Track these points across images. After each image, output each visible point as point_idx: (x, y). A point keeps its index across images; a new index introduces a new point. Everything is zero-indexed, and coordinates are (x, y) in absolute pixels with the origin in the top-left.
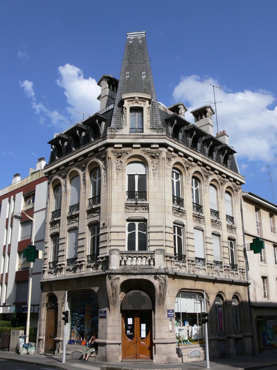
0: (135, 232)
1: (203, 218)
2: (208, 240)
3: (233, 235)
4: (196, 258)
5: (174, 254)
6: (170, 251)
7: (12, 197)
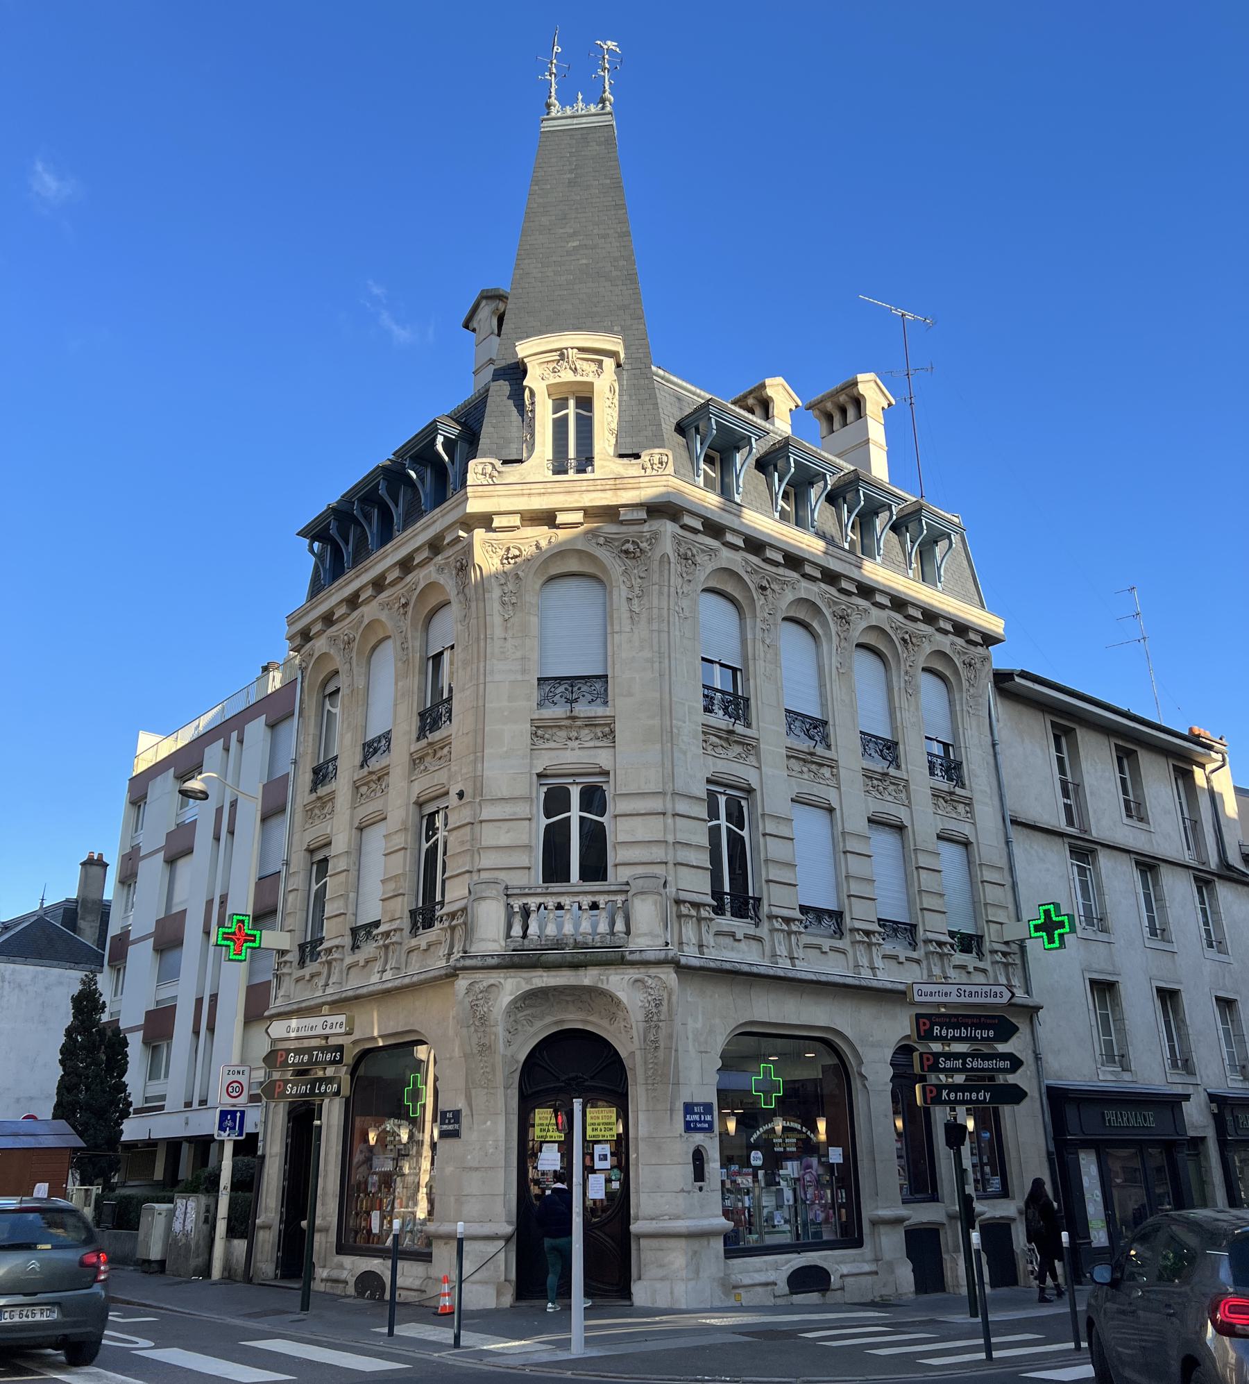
1: (832, 764)
2: (852, 845)
3: (745, 772)
4: (804, 909)
6: (698, 885)
7: (234, 735)
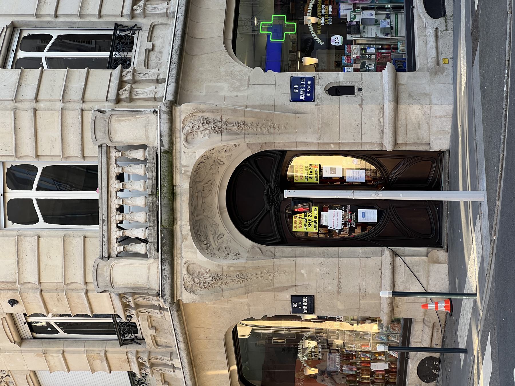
0: (37, 200)
5: (109, 71)
